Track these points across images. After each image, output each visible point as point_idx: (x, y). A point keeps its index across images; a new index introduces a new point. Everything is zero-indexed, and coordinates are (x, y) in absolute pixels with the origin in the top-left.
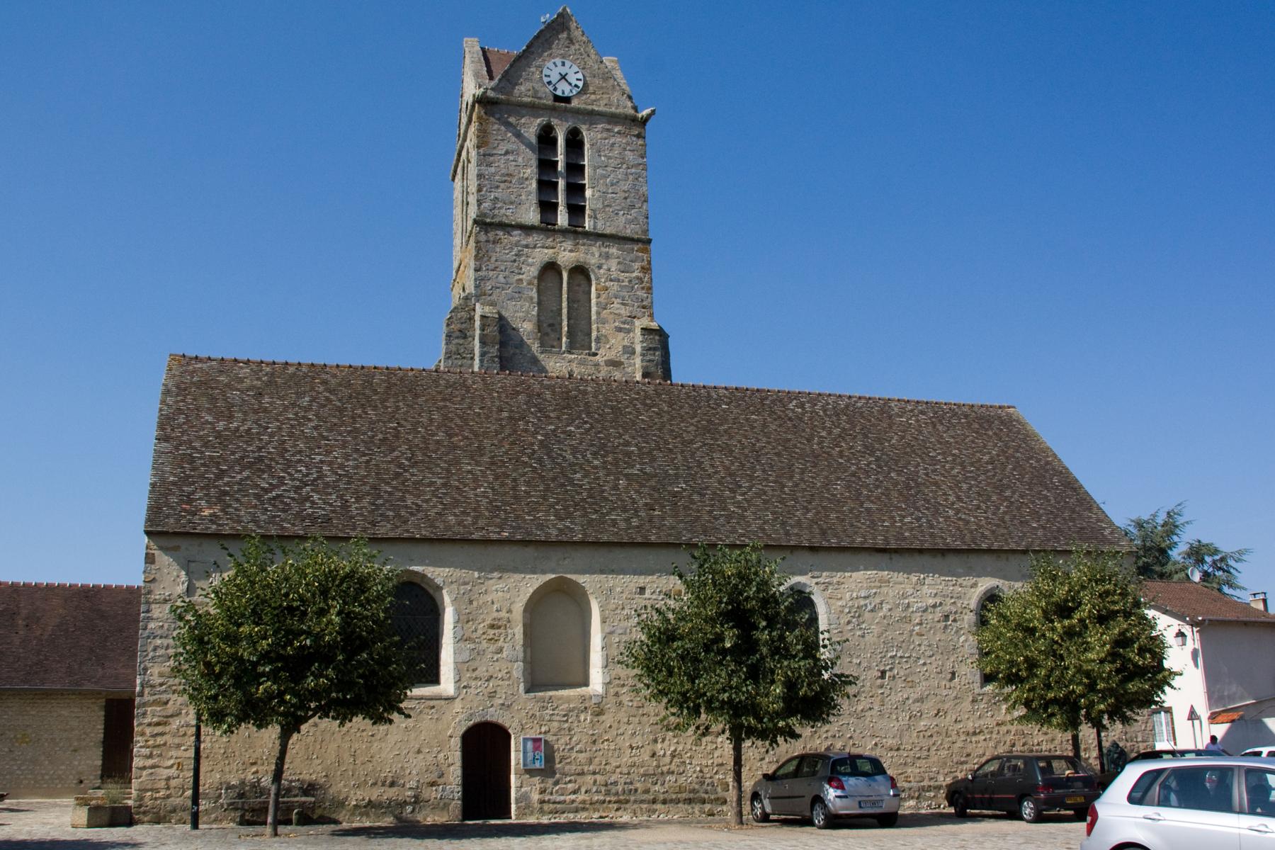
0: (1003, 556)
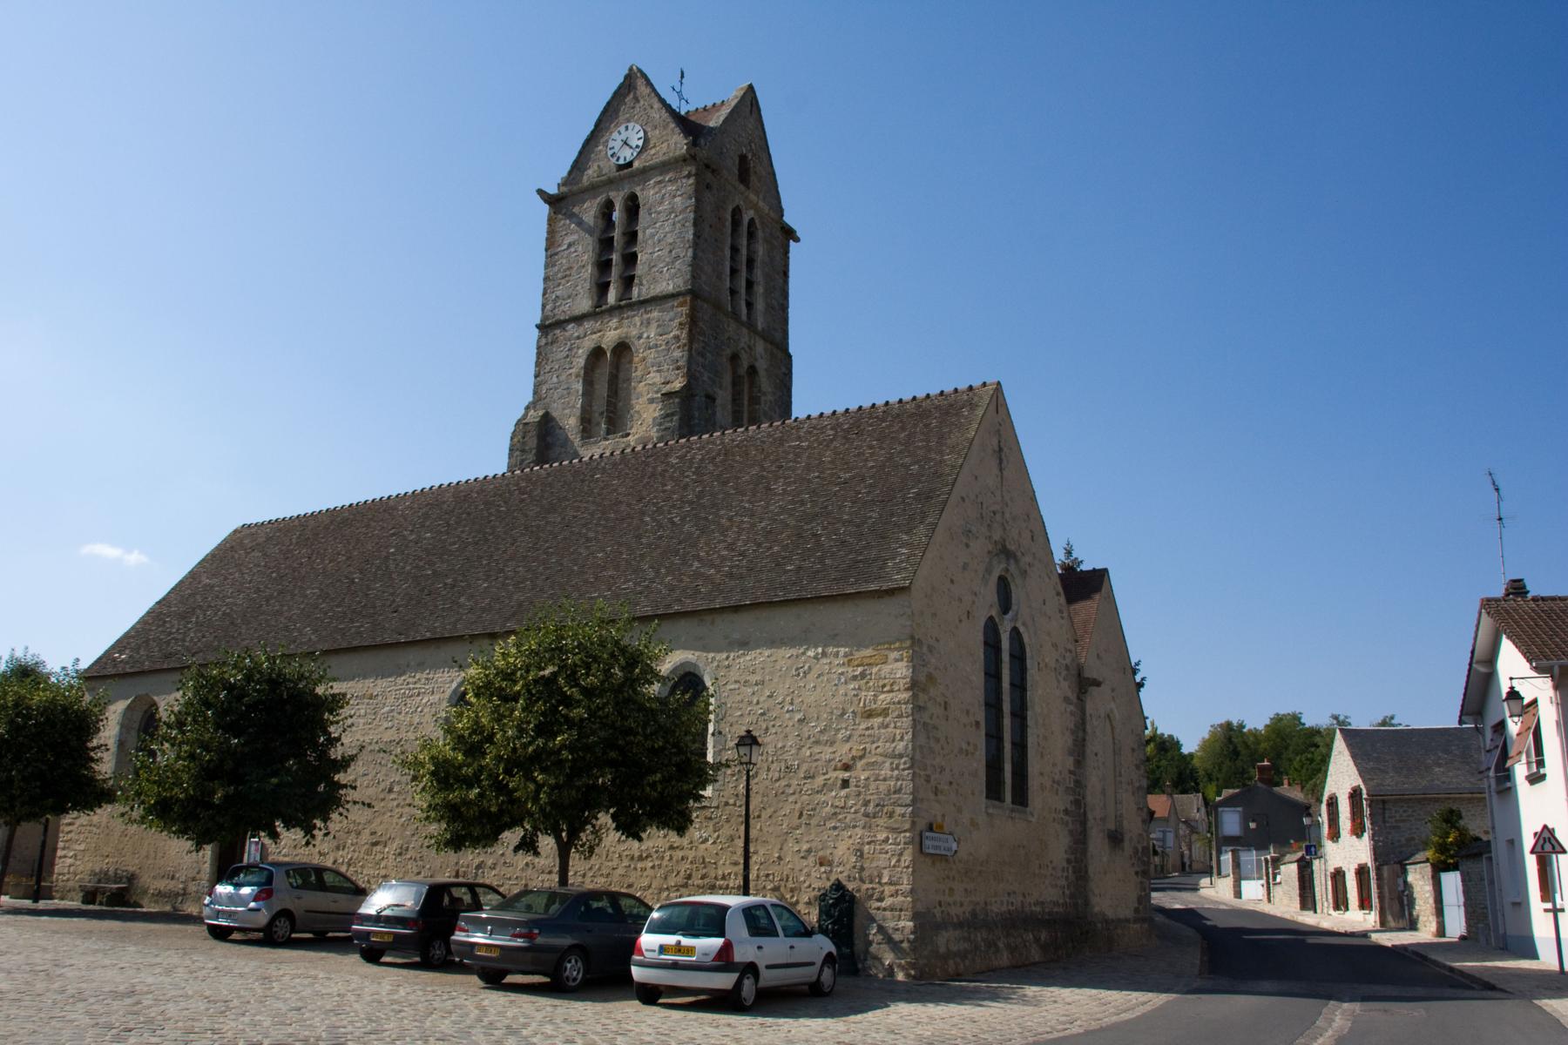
0: (708, 618)
